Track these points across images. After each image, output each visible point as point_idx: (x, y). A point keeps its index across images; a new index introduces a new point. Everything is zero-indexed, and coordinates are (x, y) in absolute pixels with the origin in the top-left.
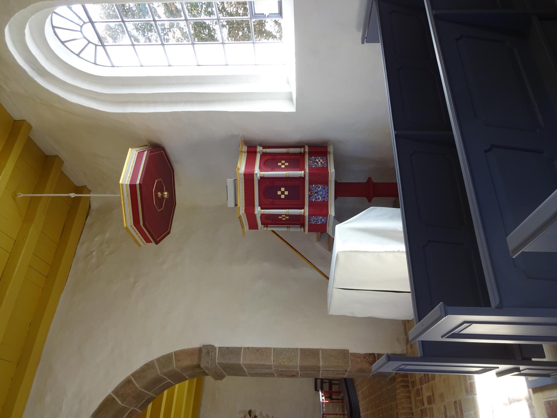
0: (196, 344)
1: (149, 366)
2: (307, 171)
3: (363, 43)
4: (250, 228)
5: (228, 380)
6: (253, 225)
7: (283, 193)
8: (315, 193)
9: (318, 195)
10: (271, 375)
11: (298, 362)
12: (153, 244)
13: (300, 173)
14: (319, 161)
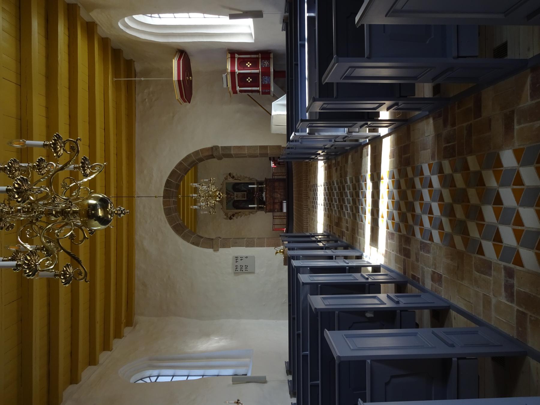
0: (209, 145)
1: (189, 156)
2: (260, 71)
3: (282, 31)
4: (234, 93)
5: (225, 160)
6: (235, 92)
7: (249, 80)
8: (265, 80)
9: (266, 81)
10: (246, 157)
11: (258, 152)
12: (188, 103)
13: (257, 71)
14: (266, 63)
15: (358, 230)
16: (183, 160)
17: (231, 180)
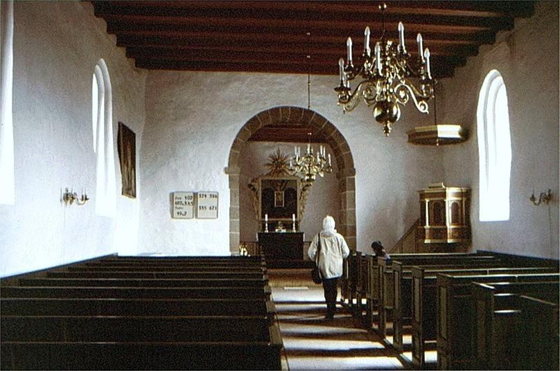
1: (342, 139)
15: (474, 255)
16: (338, 131)
17: (300, 187)
